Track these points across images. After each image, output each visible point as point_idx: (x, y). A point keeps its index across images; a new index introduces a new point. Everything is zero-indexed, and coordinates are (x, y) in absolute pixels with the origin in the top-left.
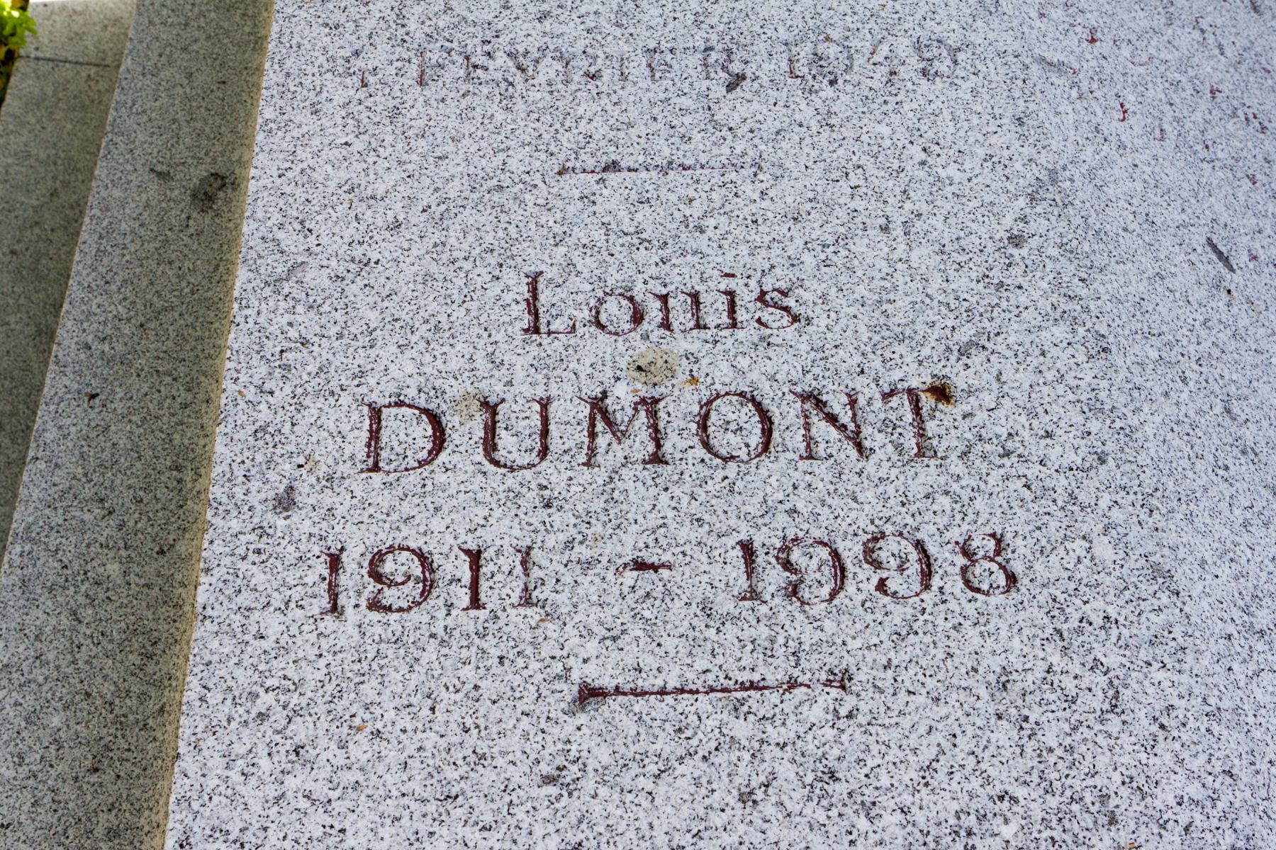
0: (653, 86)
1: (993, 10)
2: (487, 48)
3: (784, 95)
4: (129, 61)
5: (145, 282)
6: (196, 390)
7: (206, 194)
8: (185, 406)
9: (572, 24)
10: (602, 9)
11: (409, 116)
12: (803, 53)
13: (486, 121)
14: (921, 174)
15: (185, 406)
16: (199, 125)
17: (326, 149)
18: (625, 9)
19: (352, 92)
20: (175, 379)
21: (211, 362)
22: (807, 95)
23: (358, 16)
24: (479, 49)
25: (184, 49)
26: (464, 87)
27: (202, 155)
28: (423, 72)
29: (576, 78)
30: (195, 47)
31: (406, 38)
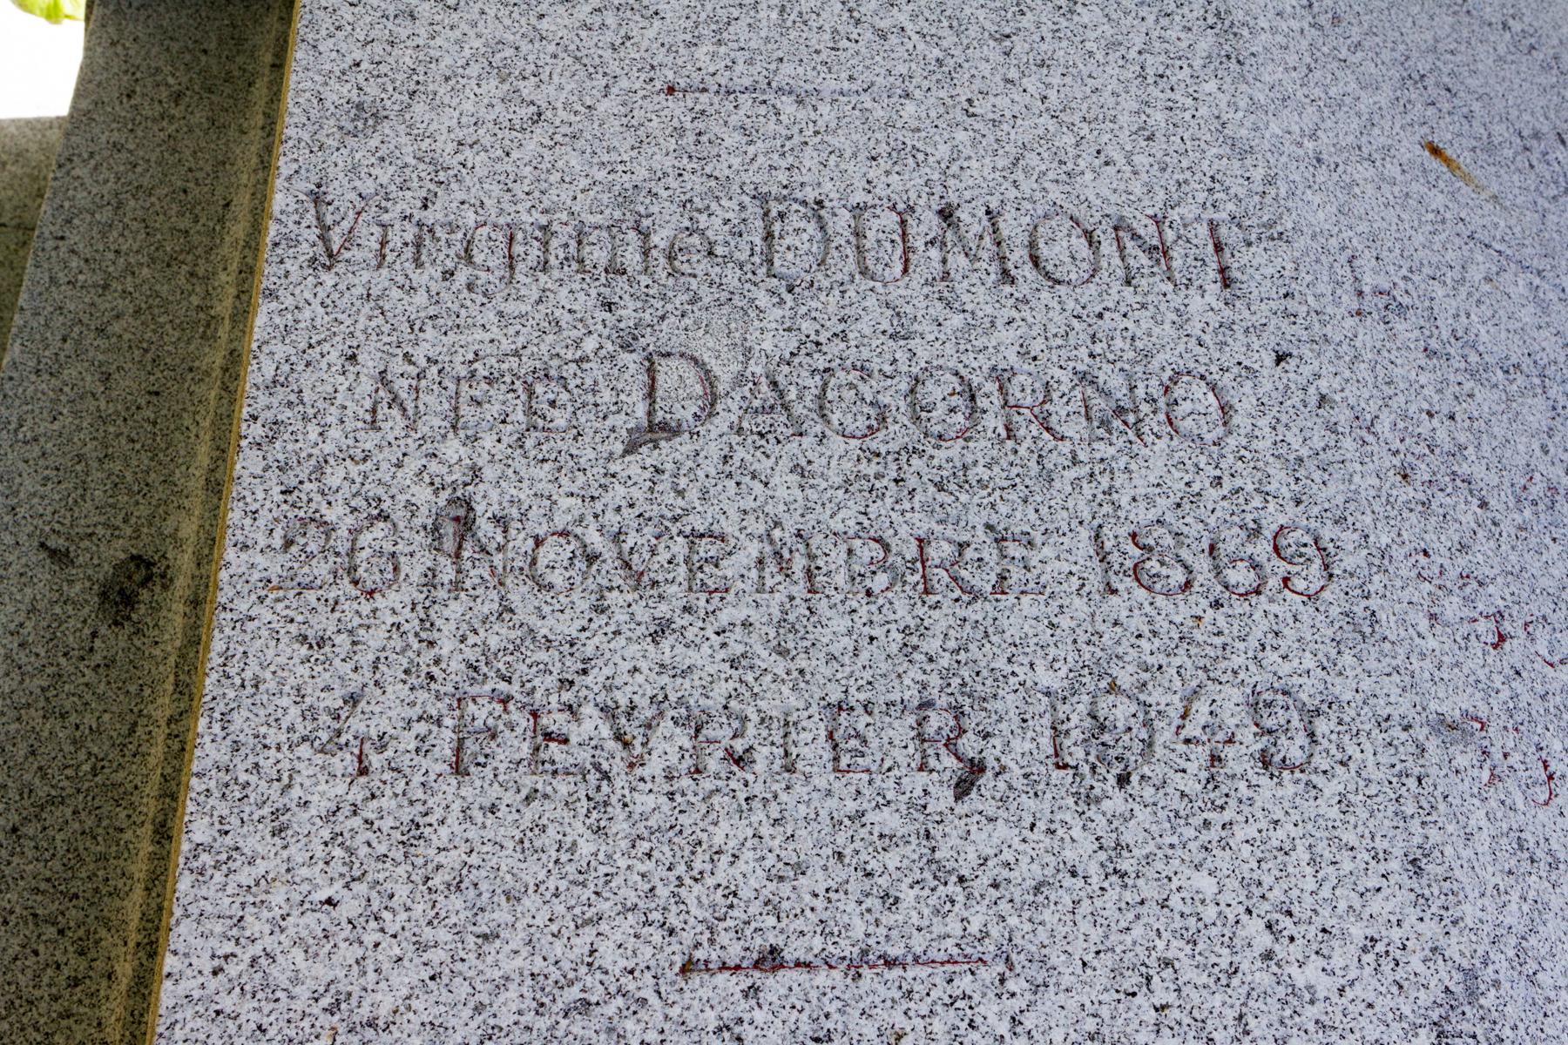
0: (837, 785)
1: (1368, 630)
2: (567, 696)
3: (1047, 806)
4: (17, 348)
5: (22, 751)
6: (92, 954)
7: (121, 592)
8: (75, 982)
9: (706, 649)
10: (755, 617)
11: (436, 843)
12: (1075, 719)
13: (564, 857)
14: (1264, 979)
15: (75, 982)
16: (117, 467)
17: (296, 912)
18: (791, 618)
19: (340, 788)
20: (61, 932)
21: (118, 903)
22: (1082, 807)
23: (357, 621)
24: (554, 699)
25: (100, 331)
26: (528, 782)
27: (118, 522)
28: (461, 741)
29: (713, 764)
30: (116, 327)
31: (435, 671)
